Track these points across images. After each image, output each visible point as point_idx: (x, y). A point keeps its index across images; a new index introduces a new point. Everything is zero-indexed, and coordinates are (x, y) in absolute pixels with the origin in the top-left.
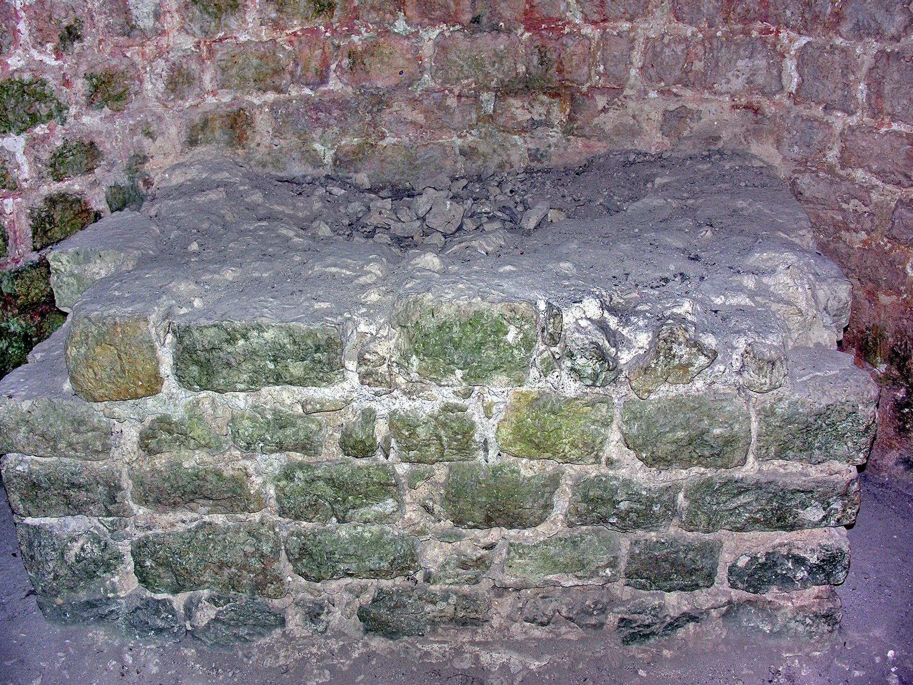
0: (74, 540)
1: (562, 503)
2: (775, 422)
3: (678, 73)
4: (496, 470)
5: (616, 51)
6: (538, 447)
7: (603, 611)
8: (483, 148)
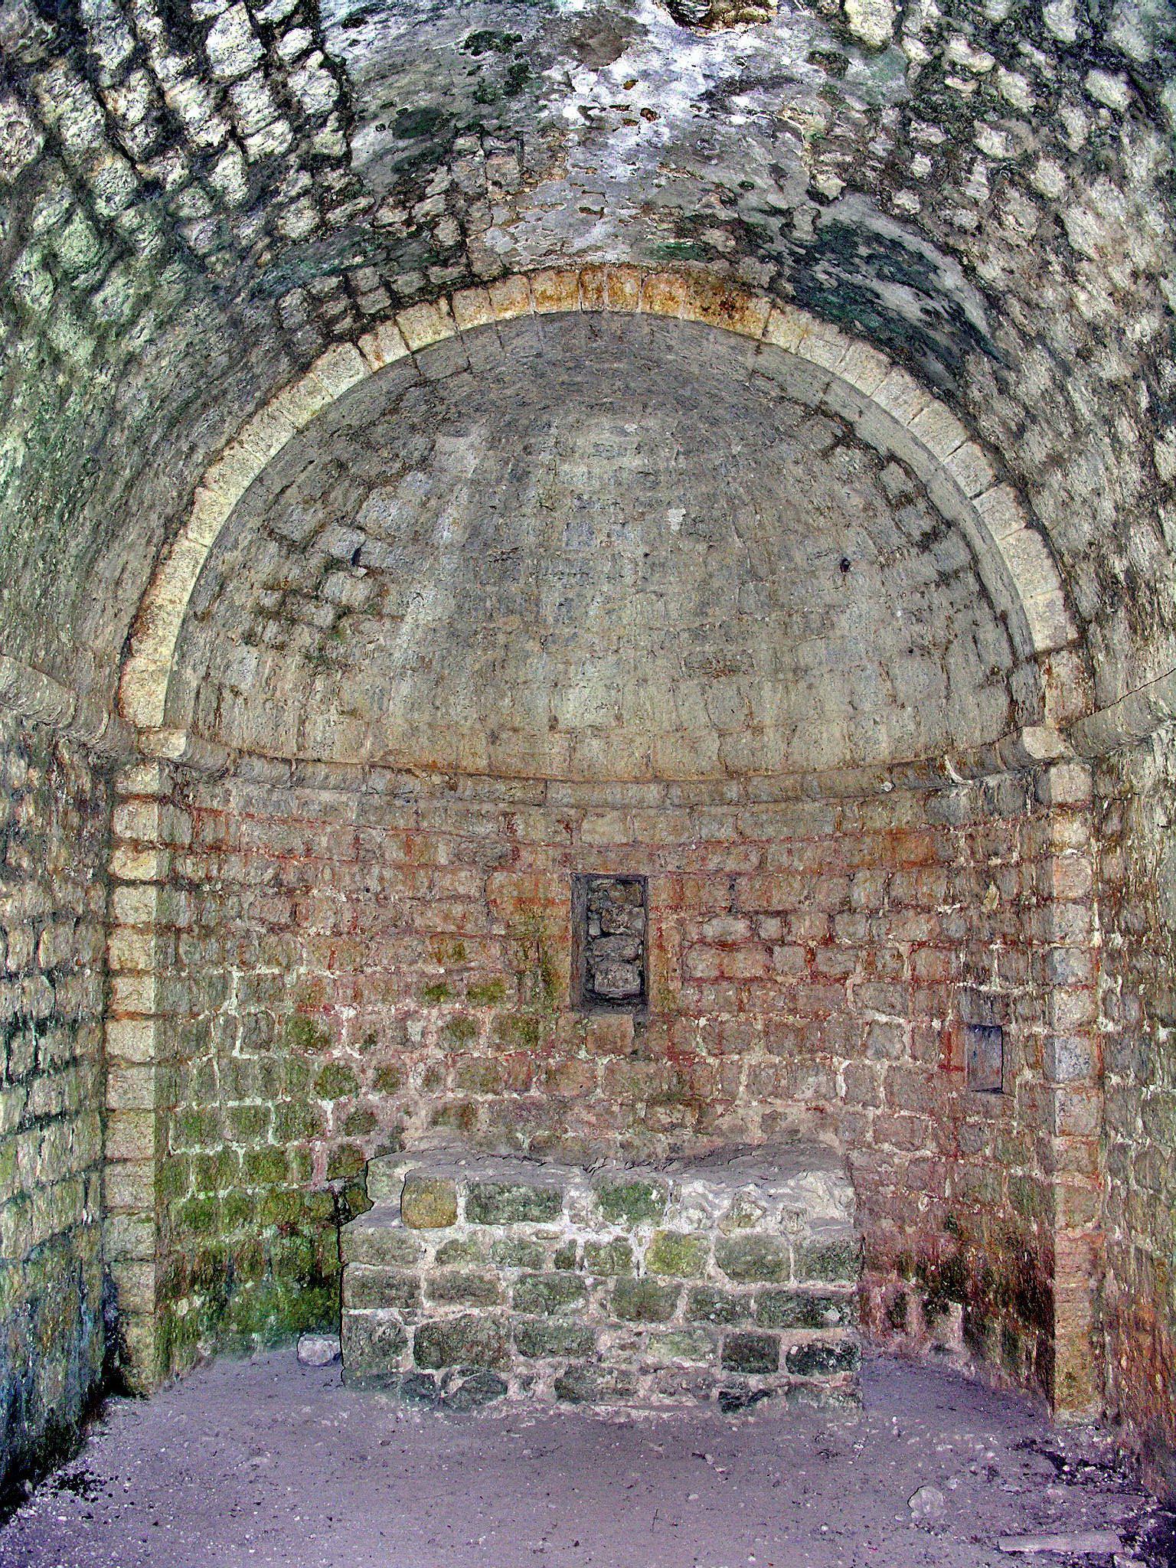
0: (380, 1325)
1: (682, 1304)
2: (803, 1252)
3: (770, 1088)
4: (644, 1282)
5: (730, 1074)
6: (668, 1265)
7: (709, 1386)
8: (637, 1142)
